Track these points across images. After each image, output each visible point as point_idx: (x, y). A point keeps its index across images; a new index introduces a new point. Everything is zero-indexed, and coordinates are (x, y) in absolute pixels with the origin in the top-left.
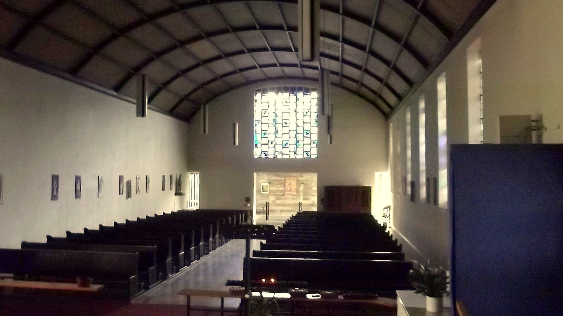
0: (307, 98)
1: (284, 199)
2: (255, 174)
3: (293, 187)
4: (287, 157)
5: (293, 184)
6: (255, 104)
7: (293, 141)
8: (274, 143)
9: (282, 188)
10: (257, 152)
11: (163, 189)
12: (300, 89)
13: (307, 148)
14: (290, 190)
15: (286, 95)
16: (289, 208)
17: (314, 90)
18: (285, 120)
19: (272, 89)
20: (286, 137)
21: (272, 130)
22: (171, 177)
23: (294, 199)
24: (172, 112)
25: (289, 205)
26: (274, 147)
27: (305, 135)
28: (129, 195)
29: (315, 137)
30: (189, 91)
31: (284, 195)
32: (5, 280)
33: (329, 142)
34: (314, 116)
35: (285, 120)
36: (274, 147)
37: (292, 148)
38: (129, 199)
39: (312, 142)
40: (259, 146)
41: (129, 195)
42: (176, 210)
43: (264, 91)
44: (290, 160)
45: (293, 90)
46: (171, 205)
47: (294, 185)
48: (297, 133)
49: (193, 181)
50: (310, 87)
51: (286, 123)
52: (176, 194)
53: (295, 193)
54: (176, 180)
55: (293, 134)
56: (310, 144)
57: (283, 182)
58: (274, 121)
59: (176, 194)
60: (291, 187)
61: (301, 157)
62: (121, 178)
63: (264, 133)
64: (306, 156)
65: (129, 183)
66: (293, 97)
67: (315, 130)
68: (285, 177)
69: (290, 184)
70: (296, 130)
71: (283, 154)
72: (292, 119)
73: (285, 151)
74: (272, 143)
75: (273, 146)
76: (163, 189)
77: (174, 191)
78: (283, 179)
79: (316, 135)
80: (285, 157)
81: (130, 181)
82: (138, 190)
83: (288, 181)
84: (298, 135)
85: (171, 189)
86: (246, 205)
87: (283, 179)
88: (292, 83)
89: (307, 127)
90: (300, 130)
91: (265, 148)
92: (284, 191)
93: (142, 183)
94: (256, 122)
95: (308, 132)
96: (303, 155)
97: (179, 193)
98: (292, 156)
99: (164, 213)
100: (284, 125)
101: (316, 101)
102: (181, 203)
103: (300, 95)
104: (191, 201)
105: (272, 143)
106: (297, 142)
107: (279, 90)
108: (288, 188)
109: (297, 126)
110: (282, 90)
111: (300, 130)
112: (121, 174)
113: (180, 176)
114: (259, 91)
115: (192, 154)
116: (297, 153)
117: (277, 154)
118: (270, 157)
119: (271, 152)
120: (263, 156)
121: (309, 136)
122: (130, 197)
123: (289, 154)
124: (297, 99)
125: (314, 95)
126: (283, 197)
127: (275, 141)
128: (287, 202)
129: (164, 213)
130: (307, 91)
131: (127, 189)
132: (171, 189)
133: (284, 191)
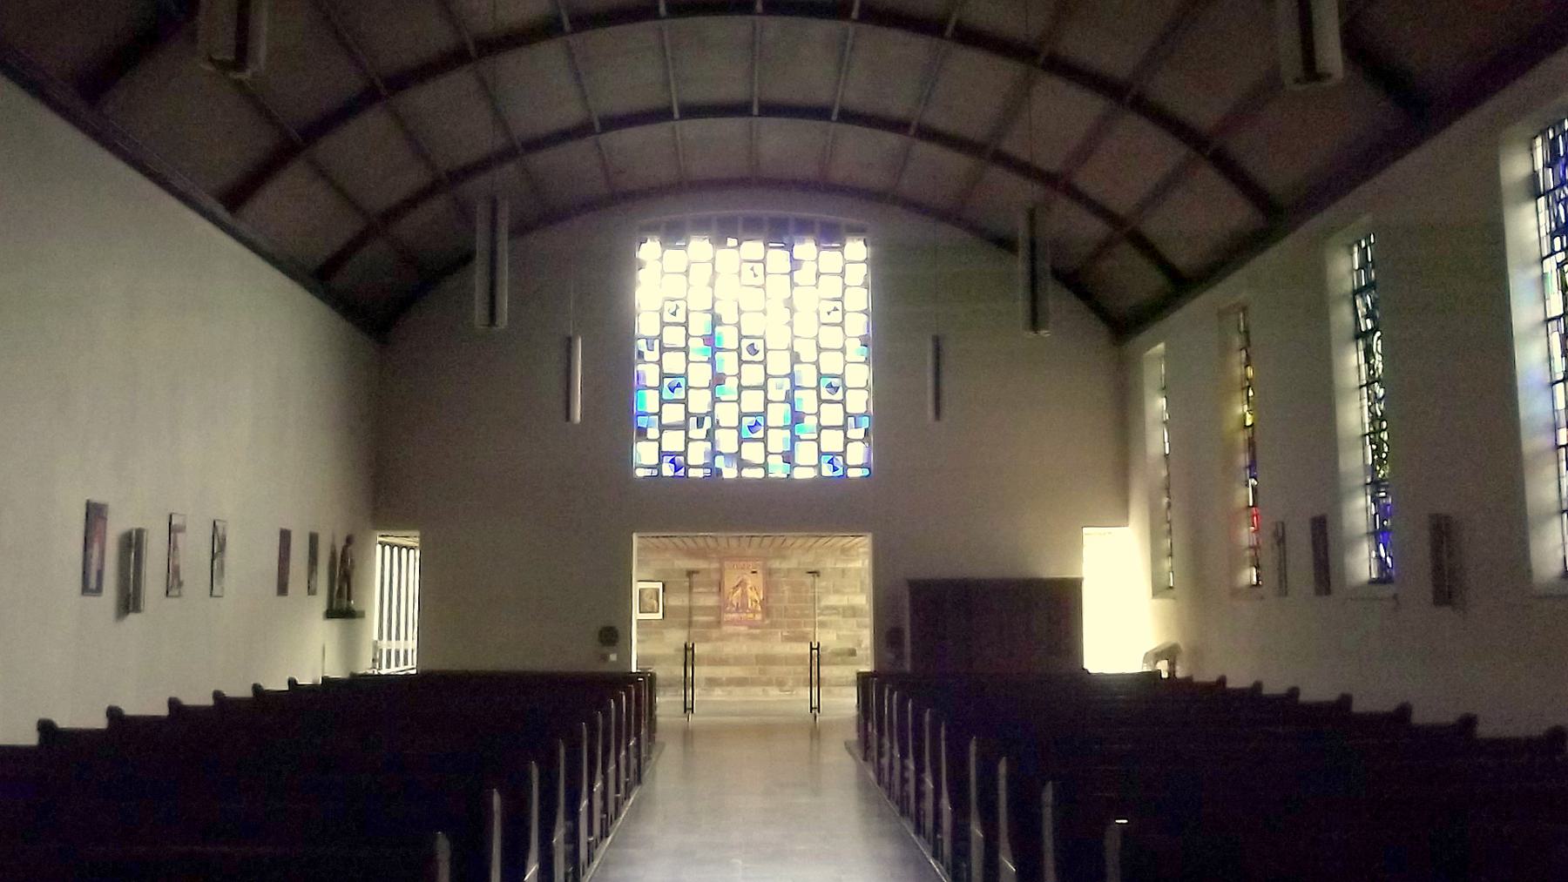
0: (831, 259)
1: (722, 639)
2: (635, 536)
3: (751, 594)
4: (758, 474)
5: (750, 583)
6: (642, 275)
7: (778, 414)
8: (708, 421)
9: (711, 601)
10: (645, 454)
11: (282, 589)
12: (804, 228)
13: (832, 441)
14: (741, 607)
15: (753, 248)
16: (737, 672)
17: (856, 231)
18: (752, 335)
19: (701, 226)
20: (753, 402)
21: (700, 375)
22: (313, 539)
23: (753, 637)
24: (320, 276)
25: (738, 661)
26: (710, 436)
27: (825, 395)
28: (129, 602)
29: (859, 402)
30: (395, 199)
31: (719, 623)
32: (1535, 295)
33: (930, 413)
34: (859, 325)
35: (752, 335)
36: (710, 436)
37: (779, 440)
38: (132, 617)
39: (851, 420)
40: (653, 433)
41: (129, 602)
42: (336, 671)
43: (673, 233)
44: (767, 483)
45: (779, 231)
46: (311, 655)
47: (754, 588)
48: (794, 387)
49: (394, 573)
50: (844, 220)
51: (753, 350)
52: (331, 614)
53: (758, 617)
54: (333, 555)
55: (777, 391)
56: (844, 427)
57: (715, 577)
58: (710, 340)
59: (331, 614)
60: (744, 594)
61: (810, 474)
62: (95, 514)
63: (673, 384)
64: (827, 471)
65: (133, 544)
66: (778, 258)
67: (860, 375)
68: (721, 560)
69: (742, 584)
70: (791, 376)
71: (742, 464)
72: (778, 338)
73: (753, 452)
74: (700, 424)
75: (702, 433)
76: (282, 589)
77: (320, 602)
78: (715, 565)
79: (864, 395)
80: (748, 473)
81: (140, 532)
82: (173, 581)
83: (730, 581)
84: (798, 393)
85: (311, 591)
86: (605, 658)
87: (715, 565)
88: (771, 202)
89: (831, 364)
90: (807, 376)
91: (673, 441)
92: (719, 610)
93: (195, 548)
94: (641, 345)
95: (836, 382)
96: (818, 467)
97: (343, 609)
98: (778, 470)
99: (292, 682)
100: (746, 356)
101: (863, 269)
102: (350, 647)
103: (806, 249)
104: (394, 645)
105: (700, 424)
106: (797, 418)
107: (725, 229)
108: (735, 598)
109: (795, 359)
110: (740, 225)
111: (807, 376)
112: (97, 498)
113: (349, 540)
114: (652, 229)
115: (390, 469)
116: (798, 460)
117: (720, 462)
118: (692, 473)
119: (697, 454)
120: (668, 470)
121: (839, 396)
122: (137, 609)
123: (764, 460)
124: (795, 264)
125: (857, 249)
126: (715, 633)
127: (711, 414)
128: (729, 649)
129: (292, 682)
130: (830, 234)
131: (123, 571)
132: (311, 591)
133: (719, 610)
